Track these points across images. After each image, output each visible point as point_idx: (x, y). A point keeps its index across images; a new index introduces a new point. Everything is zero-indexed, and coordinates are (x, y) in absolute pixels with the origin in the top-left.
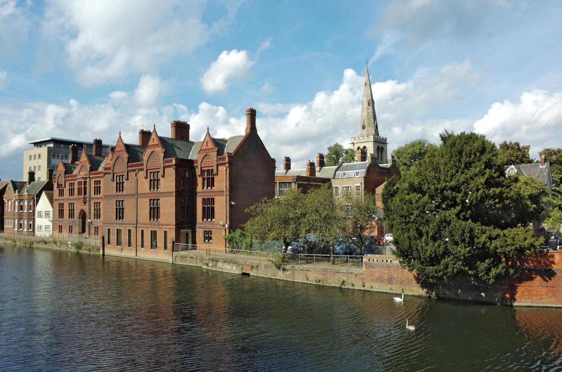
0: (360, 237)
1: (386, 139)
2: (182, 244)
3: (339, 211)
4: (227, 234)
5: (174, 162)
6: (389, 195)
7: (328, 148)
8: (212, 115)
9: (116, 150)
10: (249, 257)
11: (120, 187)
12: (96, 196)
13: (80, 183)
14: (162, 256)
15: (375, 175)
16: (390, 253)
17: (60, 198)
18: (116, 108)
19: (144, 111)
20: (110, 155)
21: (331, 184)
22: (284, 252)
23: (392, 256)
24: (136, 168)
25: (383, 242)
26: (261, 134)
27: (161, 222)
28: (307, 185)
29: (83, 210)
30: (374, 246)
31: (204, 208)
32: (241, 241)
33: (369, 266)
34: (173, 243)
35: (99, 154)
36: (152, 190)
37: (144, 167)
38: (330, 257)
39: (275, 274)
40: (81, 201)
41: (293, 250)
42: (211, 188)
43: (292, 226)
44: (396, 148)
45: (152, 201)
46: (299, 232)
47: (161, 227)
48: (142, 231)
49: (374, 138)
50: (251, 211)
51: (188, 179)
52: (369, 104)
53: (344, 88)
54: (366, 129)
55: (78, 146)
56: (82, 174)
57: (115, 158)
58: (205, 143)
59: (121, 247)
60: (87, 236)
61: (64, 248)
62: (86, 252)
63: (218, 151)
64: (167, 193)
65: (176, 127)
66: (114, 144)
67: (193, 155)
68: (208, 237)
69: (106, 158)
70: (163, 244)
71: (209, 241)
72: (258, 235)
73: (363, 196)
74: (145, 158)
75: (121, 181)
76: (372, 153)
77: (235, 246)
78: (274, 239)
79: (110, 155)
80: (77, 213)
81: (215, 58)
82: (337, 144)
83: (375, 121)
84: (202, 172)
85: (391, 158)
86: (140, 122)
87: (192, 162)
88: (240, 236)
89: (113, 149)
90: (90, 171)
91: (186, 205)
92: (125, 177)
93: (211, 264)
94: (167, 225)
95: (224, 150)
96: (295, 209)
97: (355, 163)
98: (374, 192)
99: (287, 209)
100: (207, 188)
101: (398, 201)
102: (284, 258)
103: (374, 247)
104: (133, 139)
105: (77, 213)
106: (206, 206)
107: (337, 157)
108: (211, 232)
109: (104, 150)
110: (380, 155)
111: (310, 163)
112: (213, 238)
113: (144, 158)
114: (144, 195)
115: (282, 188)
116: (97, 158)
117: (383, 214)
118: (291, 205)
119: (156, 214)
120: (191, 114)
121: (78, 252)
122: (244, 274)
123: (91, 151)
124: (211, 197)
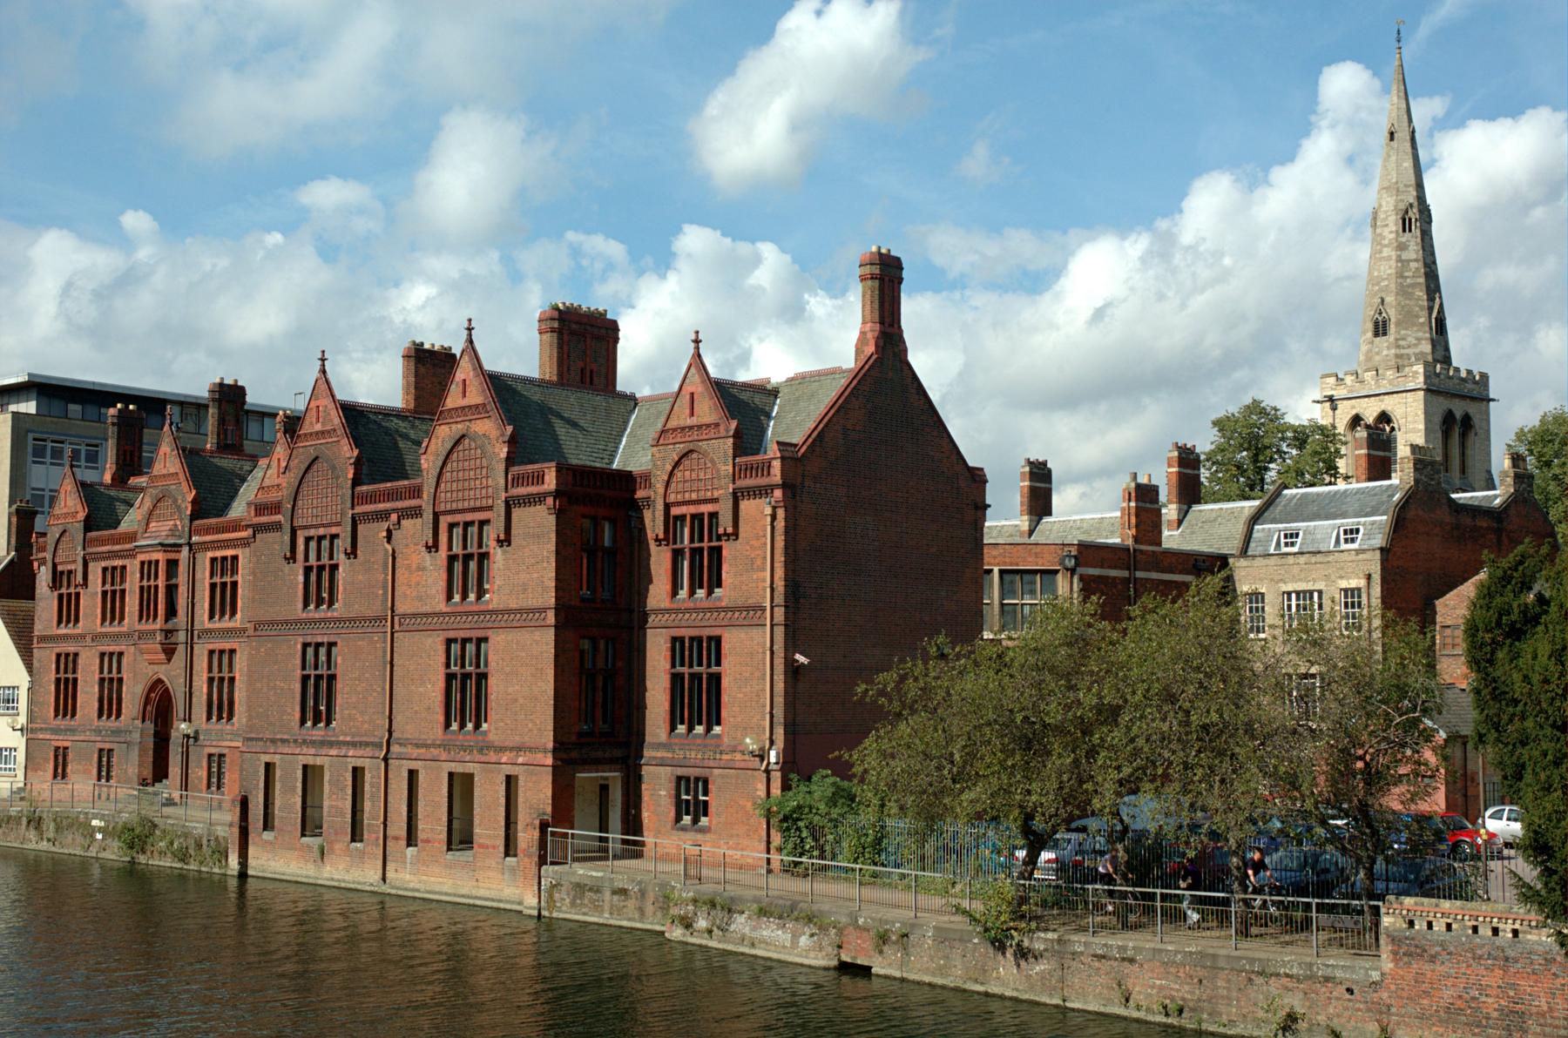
0: (1363, 815)
1: (1484, 376)
2: (583, 833)
3: (1265, 700)
4: (776, 790)
5: (550, 482)
6: (1496, 635)
7: (1215, 423)
8: (730, 275)
9: (306, 429)
10: (868, 893)
11: (320, 585)
12: (217, 624)
13: (148, 569)
14: (498, 884)
15: (1431, 541)
16: (1511, 893)
17: (63, 631)
18: (328, 252)
19: (447, 266)
20: (280, 451)
21: (1229, 579)
22: (1021, 876)
23: (1520, 910)
24: (388, 505)
25: (1473, 845)
26: (929, 362)
27: (492, 737)
28: (1126, 581)
29: (160, 681)
30: (1433, 861)
31: (676, 679)
32: (836, 823)
33: (1410, 949)
34: (543, 826)
35: (231, 444)
36: (457, 598)
37: (425, 501)
38: (1226, 902)
39: (983, 974)
40: (155, 644)
41: (1061, 867)
42: (710, 593)
43: (1060, 760)
44: (1531, 420)
45: (455, 648)
46: (1089, 786)
47: (492, 757)
48: (412, 774)
49: (1427, 377)
50: (882, 693)
51: (612, 552)
52: (1406, 225)
53: (1321, 148)
54: (1391, 337)
55: (142, 413)
56: (161, 529)
57: (299, 464)
58: (685, 399)
59: (318, 840)
60: (176, 795)
61: (72, 846)
62: (167, 862)
63: (737, 435)
64: (520, 611)
65: (559, 332)
66: (300, 405)
67: (633, 453)
68: (692, 802)
69: (263, 462)
70: (502, 833)
71: (695, 821)
72: (910, 800)
73: (1377, 635)
74: (429, 463)
75: (325, 560)
76: (1420, 440)
77: (809, 843)
78: (979, 816)
79: (280, 451)
80: (133, 694)
81: (763, 33)
82: (1256, 403)
83: (1431, 299)
84: (672, 523)
85: (1507, 463)
86: (425, 310)
87: (627, 480)
88: (832, 801)
89: (293, 424)
90: (193, 517)
91: (600, 664)
92: (343, 543)
93: (702, 923)
94: (519, 749)
95: (763, 431)
96: (1070, 688)
97: (1341, 486)
98: (1427, 618)
99: (1038, 685)
100: (692, 593)
101: (1543, 658)
102: (1023, 900)
103: (1431, 862)
104: (379, 383)
105: (133, 694)
106: (685, 670)
107: (1255, 459)
108: (706, 782)
109: (253, 428)
110: (1455, 452)
111: (1139, 487)
112: (712, 809)
113: (424, 464)
114: (422, 620)
115: (1013, 594)
116: (227, 462)
117: (1473, 714)
118: (1052, 670)
119: (70, 665)
120: (641, 273)
121: (133, 862)
122: (845, 968)
123: (199, 431)
124: (706, 632)
